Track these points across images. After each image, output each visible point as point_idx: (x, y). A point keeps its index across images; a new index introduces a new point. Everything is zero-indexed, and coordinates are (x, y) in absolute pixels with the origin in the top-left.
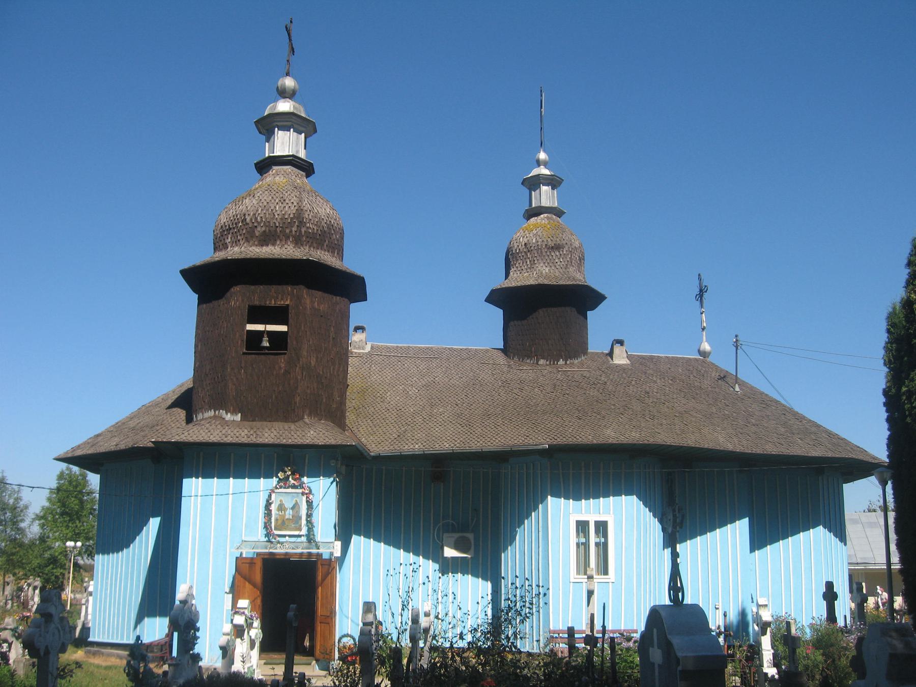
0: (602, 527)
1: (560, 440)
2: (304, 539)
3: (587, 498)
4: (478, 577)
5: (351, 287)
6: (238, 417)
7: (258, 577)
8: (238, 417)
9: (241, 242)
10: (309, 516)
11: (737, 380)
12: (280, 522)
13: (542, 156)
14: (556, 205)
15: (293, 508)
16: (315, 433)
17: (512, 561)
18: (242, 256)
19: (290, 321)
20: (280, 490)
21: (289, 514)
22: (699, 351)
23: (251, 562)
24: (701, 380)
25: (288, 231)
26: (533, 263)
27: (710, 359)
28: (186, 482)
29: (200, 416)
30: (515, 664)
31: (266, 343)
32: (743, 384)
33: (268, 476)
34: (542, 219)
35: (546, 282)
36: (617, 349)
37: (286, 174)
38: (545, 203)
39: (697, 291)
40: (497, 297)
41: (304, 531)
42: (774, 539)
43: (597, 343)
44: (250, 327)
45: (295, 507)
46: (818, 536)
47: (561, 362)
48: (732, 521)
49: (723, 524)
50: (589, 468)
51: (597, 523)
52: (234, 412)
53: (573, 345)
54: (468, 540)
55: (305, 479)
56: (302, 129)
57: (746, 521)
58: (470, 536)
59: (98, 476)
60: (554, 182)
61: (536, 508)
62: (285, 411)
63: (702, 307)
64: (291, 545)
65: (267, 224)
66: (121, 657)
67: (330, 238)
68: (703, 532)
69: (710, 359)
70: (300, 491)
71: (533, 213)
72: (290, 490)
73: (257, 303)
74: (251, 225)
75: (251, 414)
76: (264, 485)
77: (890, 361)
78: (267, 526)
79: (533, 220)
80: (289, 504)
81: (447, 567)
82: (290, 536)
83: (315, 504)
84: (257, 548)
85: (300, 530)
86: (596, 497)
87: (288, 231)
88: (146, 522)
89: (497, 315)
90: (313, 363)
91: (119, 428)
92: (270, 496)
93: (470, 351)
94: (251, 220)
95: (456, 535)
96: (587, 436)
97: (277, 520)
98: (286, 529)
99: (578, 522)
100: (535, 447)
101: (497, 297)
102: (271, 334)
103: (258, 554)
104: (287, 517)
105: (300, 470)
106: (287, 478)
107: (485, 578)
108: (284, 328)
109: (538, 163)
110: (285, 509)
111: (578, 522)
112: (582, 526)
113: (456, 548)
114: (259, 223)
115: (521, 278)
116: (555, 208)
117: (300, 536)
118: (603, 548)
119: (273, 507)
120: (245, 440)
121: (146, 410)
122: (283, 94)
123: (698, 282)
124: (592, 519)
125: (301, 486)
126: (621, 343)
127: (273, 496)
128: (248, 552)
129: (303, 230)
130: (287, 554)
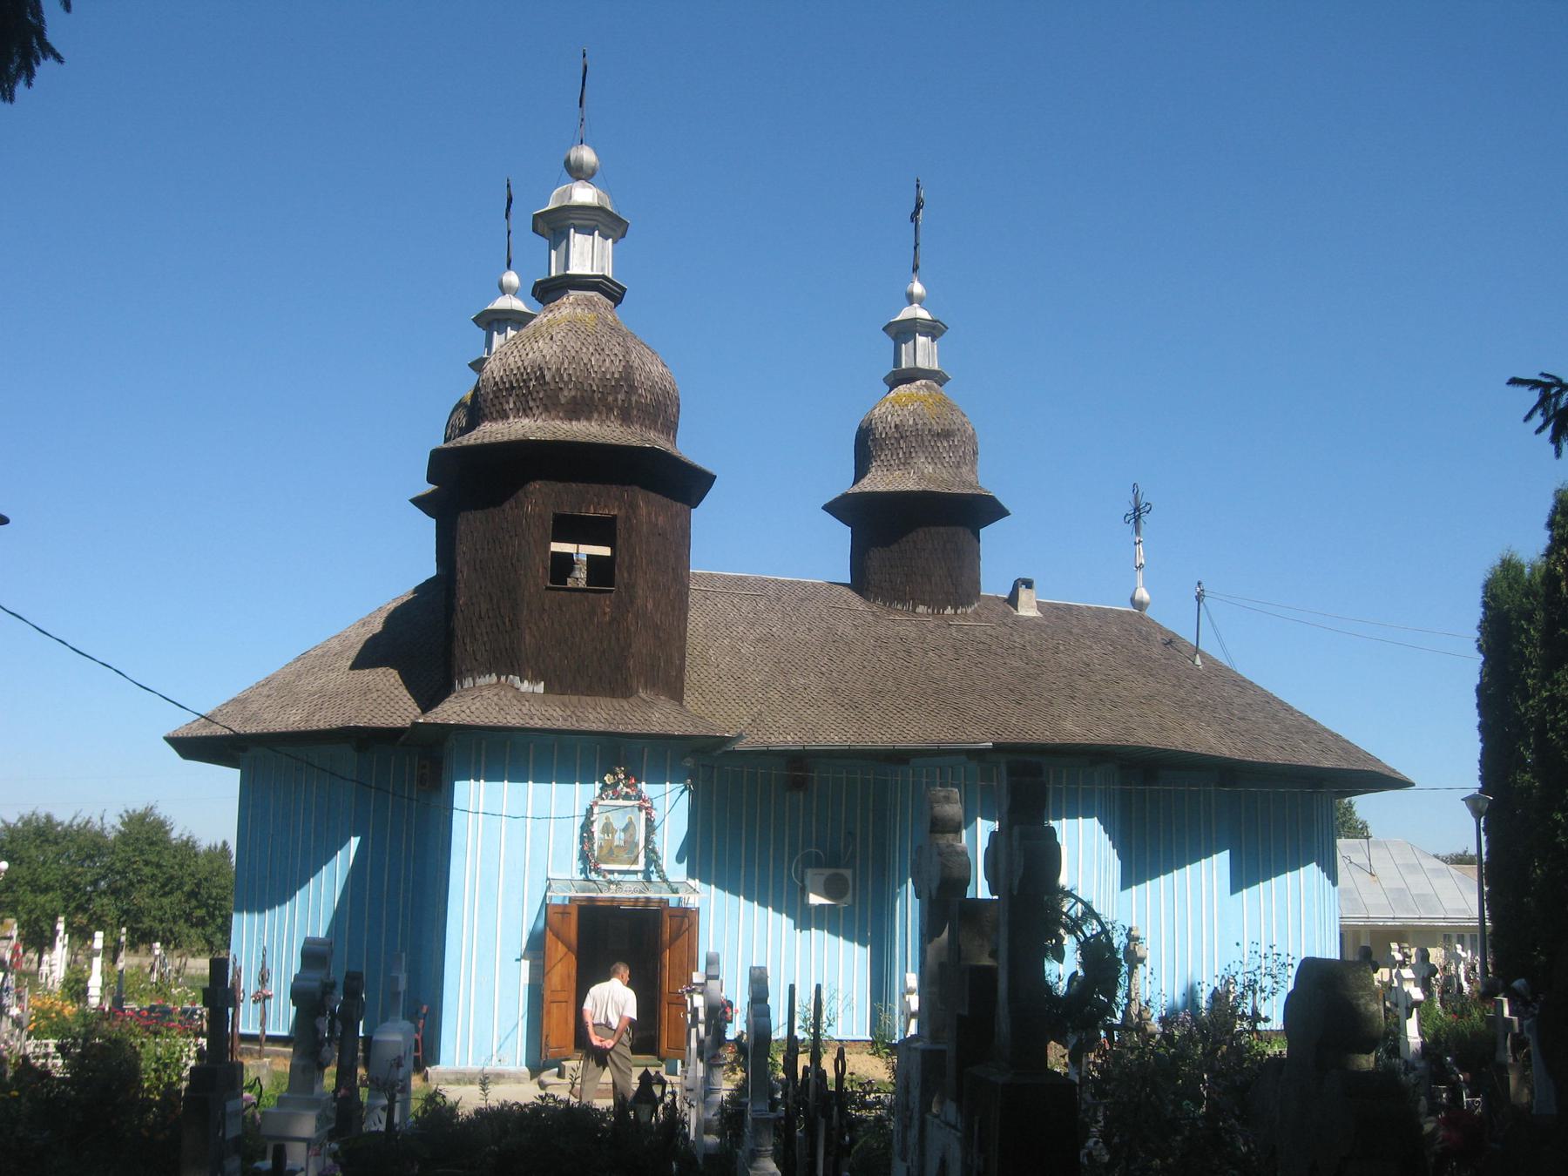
1: (1008, 737)
2: (640, 876)
4: (837, 935)
5: (688, 484)
6: (540, 688)
7: (572, 932)
8: (540, 688)
10: (648, 840)
11: (1197, 651)
12: (605, 851)
13: (918, 288)
14: (936, 367)
15: (625, 830)
16: (655, 716)
18: (548, 437)
19: (619, 542)
20: (607, 802)
21: (619, 838)
22: (1132, 600)
23: (563, 910)
24: (1136, 641)
25: (610, 399)
27: (1148, 613)
28: (457, 784)
29: (468, 683)
32: (1204, 656)
33: (587, 779)
34: (918, 388)
35: (933, 488)
36: (1024, 594)
37: (590, 304)
38: (922, 363)
39: (1130, 509)
40: (841, 508)
41: (641, 866)
43: (993, 584)
44: (556, 547)
46: (1311, 873)
47: (949, 611)
48: (1208, 854)
49: (1195, 858)
52: (534, 680)
53: (959, 585)
54: (843, 879)
55: (643, 786)
56: (609, 232)
57: (1225, 856)
58: (848, 873)
59: (238, 772)
60: (933, 330)
62: (607, 675)
63: (1137, 532)
65: (579, 385)
67: (619, 394)
68: (1168, 869)
69: (1148, 613)
71: (900, 377)
72: (621, 802)
73: (567, 511)
75: (559, 683)
76: (581, 794)
77: (1488, 648)
78: (584, 857)
80: (619, 822)
81: (806, 919)
82: (620, 872)
84: (590, 891)
85: (635, 861)
87: (610, 399)
88: (343, 842)
89: (840, 536)
90: (650, 606)
91: (278, 688)
92: (590, 811)
93: (804, 586)
95: (828, 872)
97: (601, 847)
98: (614, 862)
100: (974, 746)
101: (841, 508)
104: (616, 843)
105: (635, 774)
106: (616, 784)
107: (863, 944)
108: (605, 551)
109: (911, 299)
110: (614, 832)
113: (827, 894)
114: (566, 384)
115: (880, 481)
116: (936, 372)
119: (596, 828)
120: (560, 724)
121: (309, 664)
122: (577, 172)
123: (1131, 497)
125: (639, 797)
126: (1029, 584)
127: (596, 810)
128: (558, 897)
129: (634, 399)
130: (613, 899)
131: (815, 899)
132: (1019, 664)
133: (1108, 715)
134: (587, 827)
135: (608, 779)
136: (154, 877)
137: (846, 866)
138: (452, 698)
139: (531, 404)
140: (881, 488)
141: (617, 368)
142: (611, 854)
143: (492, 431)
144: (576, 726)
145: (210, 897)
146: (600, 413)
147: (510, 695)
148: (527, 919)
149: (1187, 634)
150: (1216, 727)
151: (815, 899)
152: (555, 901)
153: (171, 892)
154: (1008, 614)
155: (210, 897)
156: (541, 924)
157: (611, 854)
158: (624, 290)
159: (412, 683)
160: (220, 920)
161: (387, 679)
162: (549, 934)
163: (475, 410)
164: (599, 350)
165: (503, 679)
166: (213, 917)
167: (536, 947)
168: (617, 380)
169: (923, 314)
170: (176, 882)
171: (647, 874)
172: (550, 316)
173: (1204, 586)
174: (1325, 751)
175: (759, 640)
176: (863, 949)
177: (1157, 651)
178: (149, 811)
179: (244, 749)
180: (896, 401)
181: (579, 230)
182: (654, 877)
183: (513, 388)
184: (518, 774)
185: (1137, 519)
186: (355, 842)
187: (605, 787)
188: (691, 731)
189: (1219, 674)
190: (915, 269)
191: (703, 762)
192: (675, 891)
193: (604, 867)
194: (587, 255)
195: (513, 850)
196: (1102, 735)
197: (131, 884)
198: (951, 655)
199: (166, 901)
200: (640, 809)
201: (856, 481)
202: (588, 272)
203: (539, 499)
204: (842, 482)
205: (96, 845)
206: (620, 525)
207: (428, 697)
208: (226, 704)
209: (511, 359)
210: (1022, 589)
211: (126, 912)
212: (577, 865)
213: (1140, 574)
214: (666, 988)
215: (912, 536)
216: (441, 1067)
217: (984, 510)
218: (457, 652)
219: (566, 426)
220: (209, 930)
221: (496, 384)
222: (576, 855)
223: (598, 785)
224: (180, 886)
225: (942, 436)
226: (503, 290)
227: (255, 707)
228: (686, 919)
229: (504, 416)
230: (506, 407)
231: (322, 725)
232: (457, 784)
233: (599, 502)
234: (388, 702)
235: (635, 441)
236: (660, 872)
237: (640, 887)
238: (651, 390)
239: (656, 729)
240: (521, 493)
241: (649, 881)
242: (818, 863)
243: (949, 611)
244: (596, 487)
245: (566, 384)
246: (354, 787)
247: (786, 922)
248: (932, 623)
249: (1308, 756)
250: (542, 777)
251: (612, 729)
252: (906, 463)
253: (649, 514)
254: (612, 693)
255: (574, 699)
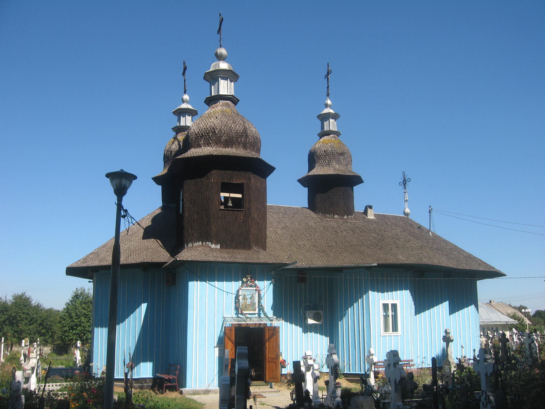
0: (394, 306)
2: (257, 315)
3: (387, 292)
6: (218, 247)
8: (218, 247)
9: (212, 144)
12: (244, 306)
13: (329, 102)
15: (251, 298)
17: (346, 325)
19: (245, 193)
20: (244, 288)
21: (249, 302)
22: (404, 213)
23: (230, 329)
25: (239, 140)
26: (330, 162)
27: (410, 217)
28: (191, 284)
29: (190, 245)
30: (411, 375)
31: (230, 204)
33: (236, 280)
34: (331, 138)
36: (369, 211)
37: (227, 105)
38: (332, 128)
39: (402, 180)
40: (303, 181)
41: (257, 312)
42: (424, 310)
43: (359, 207)
45: (252, 298)
46: (472, 308)
47: (346, 217)
48: (442, 303)
49: (437, 304)
50: (388, 276)
51: (392, 304)
52: (216, 244)
54: (319, 314)
55: (257, 282)
56: (232, 79)
57: (447, 303)
58: (321, 312)
60: (335, 117)
61: (361, 297)
63: (405, 188)
64: (252, 319)
65: (228, 135)
66: (121, 386)
67: (243, 138)
69: (410, 217)
70: (255, 288)
71: (323, 134)
72: (249, 288)
74: (218, 135)
75: (225, 245)
76: (234, 286)
78: (237, 309)
79: (325, 138)
81: (307, 329)
82: (249, 314)
83: (262, 296)
85: (255, 310)
86: (392, 291)
87: (239, 140)
88: (139, 305)
89: (304, 192)
92: (238, 291)
93: (293, 209)
94: (219, 132)
95: (314, 312)
96: (391, 260)
98: (247, 310)
99: (383, 304)
100: (368, 265)
101: (303, 181)
102: (233, 199)
103: (232, 324)
105: (254, 278)
106: (247, 282)
107: (326, 336)
108: (240, 196)
109: (327, 106)
110: (247, 299)
111: (383, 304)
112: (385, 306)
115: (318, 171)
117: (255, 314)
118: (395, 317)
119: (241, 298)
120: (228, 260)
122: (220, 58)
123: (402, 177)
124: (390, 302)
125: (256, 286)
126: (371, 207)
127: (240, 291)
128: (228, 324)
129: (248, 140)
130: (247, 324)
131: (311, 321)
132: (375, 235)
133: (411, 253)
134: (237, 297)
135: (244, 280)
136: (26, 319)
137: (319, 310)
138: (185, 250)
139: (210, 142)
140: (321, 173)
141: (241, 129)
142: (246, 307)
143: (193, 152)
144: (234, 260)
145: (47, 325)
146: (236, 145)
147: (208, 249)
148: (217, 333)
149: (426, 225)
150: (445, 257)
151: (311, 321)
152: (227, 325)
153: (33, 324)
154: (365, 218)
155: (47, 325)
156: (222, 334)
157: (246, 307)
158: (239, 100)
159: (166, 246)
160: (50, 334)
161: (154, 244)
162: (226, 338)
163: (187, 145)
164: (234, 122)
165: (204, 243)
166: (48, 332)
167: (221, 343)
168: (242, 133)
169: (332, 111)
170: (35, 320)
171: (259, 314)
172: (213, 110)
173: (432, 207)
174: (479, 265)
175: (283, 228)
176: (326, 338)
177: (416, 230)
178: (23, 295)
179: (97, 271)
180: (324, 142)
181: (223, 78)
182: (262, 316)
183: (203, 136)
184: (212, 278)
185: (405, 185)
186: (144, 306)
187: (243, 282)
188: (274, 261)
189: (436, 238)
190: (328, 95)
191: (277, 273)
192: (271, 321)
193: (244, 312)
194: (225, 87)
195: (212, 309)
196: (412, 260)
197: (18, 321)
198: (351, 233)
199: (31, 327)
200: (256, 290)
201: (310, 170)
202: (226, 94)
203: (216, 177)
204: (304, 172)
205: (4, 307)
206: (245, 186)
207: (174, 250)
208: (90, 254)
209: (201, 126)
210: (368, 209)
211: (16, 332)
212: (234, 312)
213: (406, 204)
214: (267, 356)
215: (330, 190)
216: (187, 389)
217: (356, 180)
218: (185, 233)
219: (224, 150)
220: (47, 337)
221: (196, 134)
222: (233, 308)
223: (240, 282)
224: (36, 321)
225: (341, 155)
226: (183, 101)
227: (103, 255)
228: (275, 331)
229: (200, 146)
230: (200, 143)
231: (133, 262)
232: (191, 284)
233: (237, 178)
234: (156, 252)
235: (250, 155)
236: (265, 314)
237: (257, 319)
238: (252, 137)
239: (262, 261)
240: (209, 175)
241: (260, 317)
242: (310, 308)
243: (346, 217)
244: (236, 172)
245: (223, 134)
246: (140, 286)
247: (299, 329)
248: (341, 221)
249: (464, 266)
250: (221, 279)
251: (247, 261)
252: (329, 164)
253: (254, 182)
254: (244, 248)
255: (231, 250)
